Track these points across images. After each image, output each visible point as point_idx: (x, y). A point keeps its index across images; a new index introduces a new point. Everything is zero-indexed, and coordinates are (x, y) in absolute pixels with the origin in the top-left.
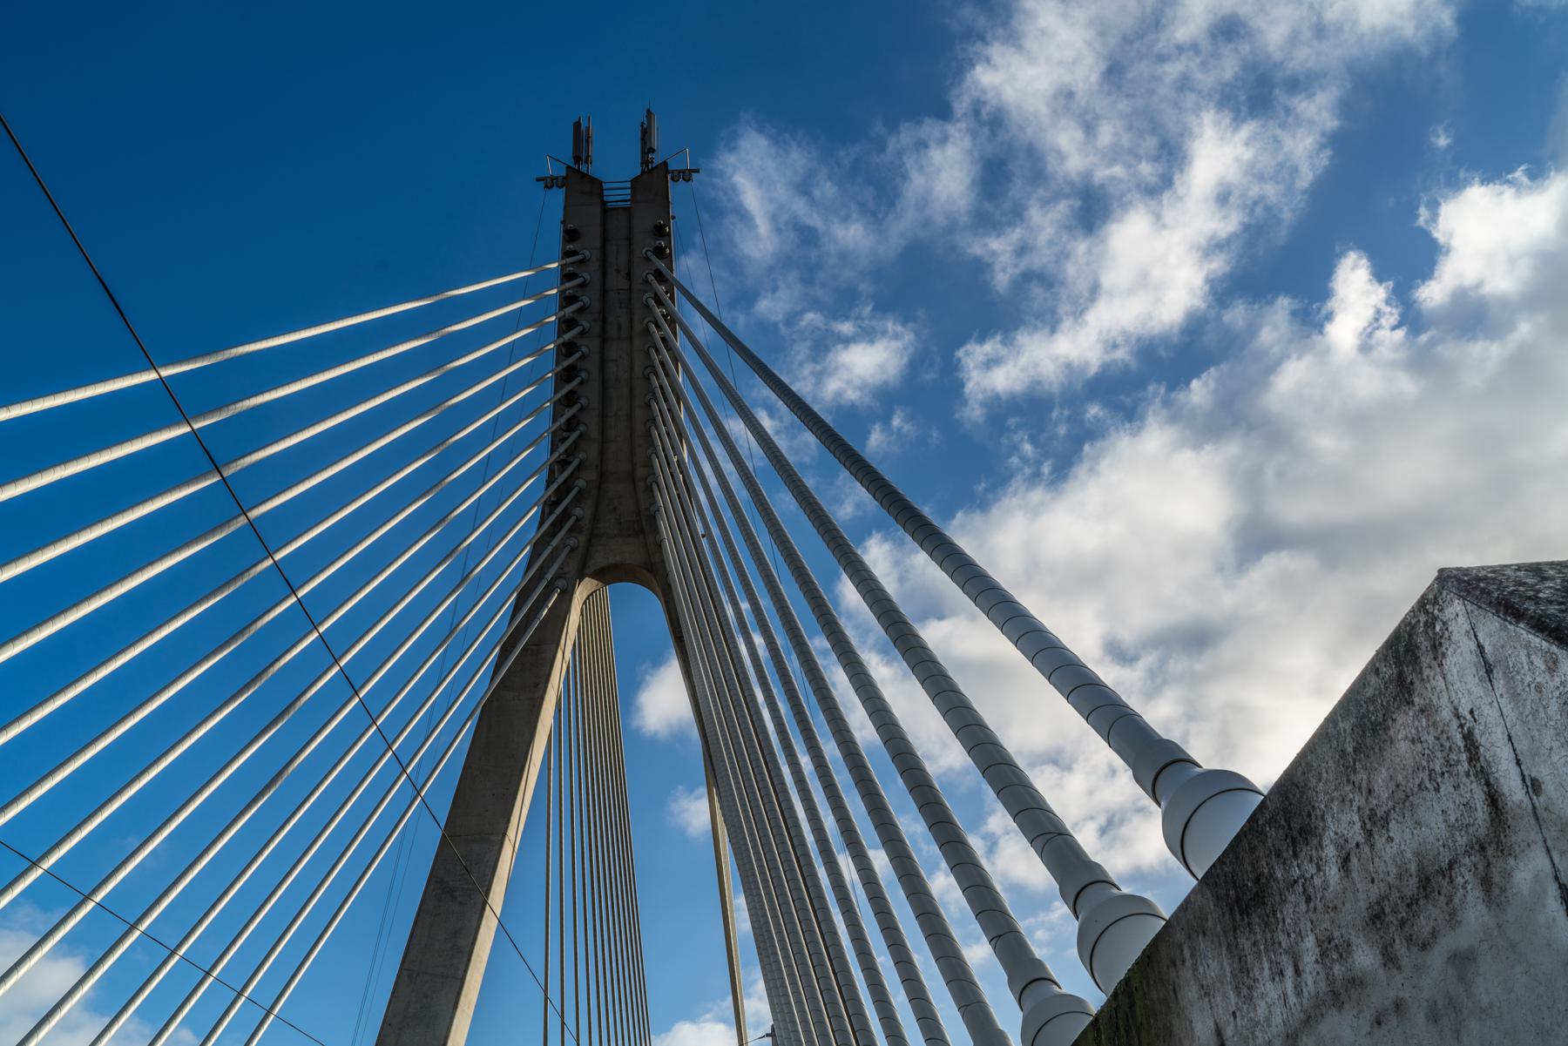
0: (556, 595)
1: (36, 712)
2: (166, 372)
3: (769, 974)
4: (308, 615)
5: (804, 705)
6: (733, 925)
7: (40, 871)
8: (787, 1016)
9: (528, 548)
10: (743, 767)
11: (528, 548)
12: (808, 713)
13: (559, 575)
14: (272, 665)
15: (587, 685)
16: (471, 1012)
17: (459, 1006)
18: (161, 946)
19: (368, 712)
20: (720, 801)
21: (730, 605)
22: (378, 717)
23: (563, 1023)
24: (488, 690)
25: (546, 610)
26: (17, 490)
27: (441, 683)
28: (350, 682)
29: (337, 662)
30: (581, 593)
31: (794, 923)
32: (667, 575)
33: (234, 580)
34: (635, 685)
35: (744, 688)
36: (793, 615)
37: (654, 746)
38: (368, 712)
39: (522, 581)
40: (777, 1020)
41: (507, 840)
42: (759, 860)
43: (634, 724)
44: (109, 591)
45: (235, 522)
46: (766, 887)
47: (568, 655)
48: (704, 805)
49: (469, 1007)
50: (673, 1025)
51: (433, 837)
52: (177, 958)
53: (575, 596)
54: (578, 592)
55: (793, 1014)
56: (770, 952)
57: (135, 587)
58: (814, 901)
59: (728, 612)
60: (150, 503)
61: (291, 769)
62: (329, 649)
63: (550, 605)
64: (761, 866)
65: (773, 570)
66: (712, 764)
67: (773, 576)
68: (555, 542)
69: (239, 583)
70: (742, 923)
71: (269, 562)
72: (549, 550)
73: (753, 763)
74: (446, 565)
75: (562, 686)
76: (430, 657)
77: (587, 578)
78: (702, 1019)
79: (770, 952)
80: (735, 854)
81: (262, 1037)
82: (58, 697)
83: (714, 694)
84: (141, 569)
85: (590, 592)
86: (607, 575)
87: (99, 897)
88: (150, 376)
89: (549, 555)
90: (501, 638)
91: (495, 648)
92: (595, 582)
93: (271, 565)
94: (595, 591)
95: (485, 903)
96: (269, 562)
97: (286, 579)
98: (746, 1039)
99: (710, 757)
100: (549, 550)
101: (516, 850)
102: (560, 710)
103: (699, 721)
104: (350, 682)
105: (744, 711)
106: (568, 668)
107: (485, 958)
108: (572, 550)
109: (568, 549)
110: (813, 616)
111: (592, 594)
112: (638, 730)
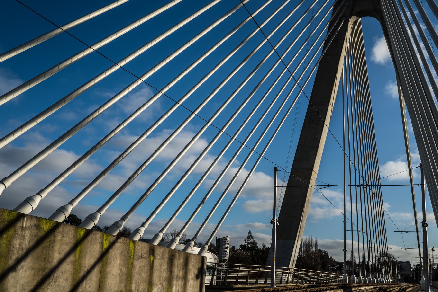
0: (343, 23)
1: (182, 74)
2: (59, 31)
3: (419, 144)
4: (264, 34)
5: (426, 37)
6: (412, 175)
7: (194, 115)
8: (428, 166)
9: (332, 7)
10: (413, 84)
11: (332, 7)
12: (428, 42)
13: (343, 16)
14: (253, 51)
15: (354, 53)
16: (321, 158)
17: (317, 156)
18: (229, 136)
19: (284, 64)
20: (402, 90)
21: (402, 12)
22: (288, 65)
23: (350, 160)
24: (326, 37)
25: (340, 28)
26: (144, 20)
27: (308, 52)
28: (278, 55)
29: (273, 48)
30: (351, 21)
31: (429, 130)
32: (382, 12)
33: (239, 25)
34: (370, 52)
35: (413, 54)
36: (430, 22)
37: (379, 66)
38: (284, 64)
39: (331, 19)
40: (423, 162)
41: (330, 105)
42: (416, 107)
43: (372, 59)
44: (209, 27)
45: (238, 6)
46: (418, 114)
47: (348, 43)
48: (396, 87)
49: (320, 156)
50: (387, 162)
51: (306, 103)
52: (234, 140)
53: (349, 22)
54: (350, 21)
55: (428, 159)
56: (422, 145)
57: (211, 30)
58: (432, 108)
59: (403, 14)
60: (202, 10)
61: (261, 83)
62: (271, 44)
63: (341, 26)
64: (417, 111)
65: (420, 2)
66: (400, 80)
67: (420, 4)
68: (341, 4)
69: (241, 26)
70: (410, 129)
71: (250, 18)
72: (340, 7)
73: (416, 81)
74: (305, 15)
75: (346, 53)
76: (302, 46)
77: (353, 16)
78: (397, 160)
79: (422, 145)
80: (408, 110)
81: (258, 165)
82: (176, 79)
83: (400, 53)
84: (189, 41)
85: (356, 20)
86: (360, 15)
87: (211, 122)
88: (65, 28)
89: (340, 9)
90: (325, 39)
91: (323, 42)
92: (356, 17)
93: (251, 19)
94: (356, 20)
95: (324, 123)
96: (250, 18)
97: (256, 22)
98: (411, 167)
99: (399, 75)
100: (340, 7)
101: (333, 108)
102: (346, 62)
103: (393, 60)
104: (278, 55)
105: (408, 49)
106: (348, 47)
107: (324, 141)
108: (347, 7)
109: (346, 6)
110: (431, 10)
111: (355, 21)
112: (373, 61)
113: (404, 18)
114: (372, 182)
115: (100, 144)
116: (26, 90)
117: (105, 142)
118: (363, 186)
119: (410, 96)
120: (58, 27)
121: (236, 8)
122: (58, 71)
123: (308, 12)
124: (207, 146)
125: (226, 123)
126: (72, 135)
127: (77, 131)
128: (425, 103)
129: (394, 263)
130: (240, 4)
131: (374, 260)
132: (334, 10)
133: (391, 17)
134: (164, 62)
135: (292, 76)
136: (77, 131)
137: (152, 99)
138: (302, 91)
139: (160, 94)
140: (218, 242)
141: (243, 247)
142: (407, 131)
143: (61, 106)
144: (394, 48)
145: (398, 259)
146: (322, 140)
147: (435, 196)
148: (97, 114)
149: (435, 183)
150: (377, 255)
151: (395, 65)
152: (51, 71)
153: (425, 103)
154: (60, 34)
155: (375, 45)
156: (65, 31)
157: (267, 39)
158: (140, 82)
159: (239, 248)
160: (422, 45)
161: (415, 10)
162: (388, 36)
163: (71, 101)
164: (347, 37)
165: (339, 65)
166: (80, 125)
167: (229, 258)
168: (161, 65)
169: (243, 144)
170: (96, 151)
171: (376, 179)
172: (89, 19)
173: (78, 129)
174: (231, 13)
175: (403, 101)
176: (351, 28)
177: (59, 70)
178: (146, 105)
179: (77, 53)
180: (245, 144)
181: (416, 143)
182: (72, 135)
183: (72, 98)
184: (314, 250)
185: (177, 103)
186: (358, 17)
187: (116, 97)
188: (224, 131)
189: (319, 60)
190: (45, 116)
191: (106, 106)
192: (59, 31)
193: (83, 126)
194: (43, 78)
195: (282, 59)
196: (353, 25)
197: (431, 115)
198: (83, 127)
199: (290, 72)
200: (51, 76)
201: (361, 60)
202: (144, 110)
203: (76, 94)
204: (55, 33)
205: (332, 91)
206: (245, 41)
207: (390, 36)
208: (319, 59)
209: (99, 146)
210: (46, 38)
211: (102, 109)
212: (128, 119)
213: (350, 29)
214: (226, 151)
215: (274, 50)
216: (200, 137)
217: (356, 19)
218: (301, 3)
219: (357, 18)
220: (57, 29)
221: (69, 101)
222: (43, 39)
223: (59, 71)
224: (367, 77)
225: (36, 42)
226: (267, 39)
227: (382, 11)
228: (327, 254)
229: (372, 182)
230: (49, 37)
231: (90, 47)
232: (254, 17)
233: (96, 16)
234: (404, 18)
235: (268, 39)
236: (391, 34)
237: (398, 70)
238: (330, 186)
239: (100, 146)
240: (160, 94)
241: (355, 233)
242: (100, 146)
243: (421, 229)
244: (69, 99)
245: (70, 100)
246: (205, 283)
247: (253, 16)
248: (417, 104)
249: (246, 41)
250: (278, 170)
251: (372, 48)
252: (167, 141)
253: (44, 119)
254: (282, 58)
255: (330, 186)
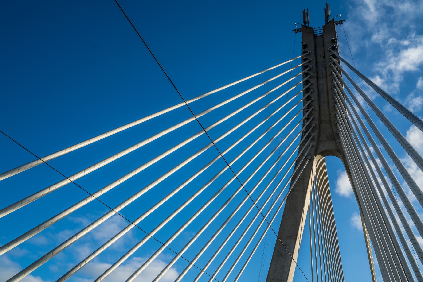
0: (308, 161)
2: (40, 162)
9: (298, 147)
11: (298, 147)
13: (308, 155)
18: (199, 269)
19: (252, 200)
24: (289, 192)
25: (305, 166)
28: (246, 191)
31: (381, 232)
34: (334, 185)
37: (343, 198)
41: (297, 239)
42: (379, 242)
43: (337, 191)
47: (313, 180)
51: (274, 238)
53: (314, 161)
54: (315, 160)
60: (168, 151)
63: (306, 164)
64: (372, 221)
66: (363, 213)
68: (307, 144)
71: (220, 156)
72: (305, 147)
75: (312, 189)
77: (318, 155)
83: (365, 198)
86: (324, 154)
91: (290, 178)
92: (320, 156)
94: (321, 159)
96: (220, 156)
100: (305, 147)
101: (301, 241)
102: (312, 197)
104: (246, 191)
106: (313, 184)
108: (312, 146)
111: (320, 160)
112: (338, 194)
113: (361, 154)
115: (69, 274)
116: (1, 217)
117: (74, 272)
119: (374, 232)
120: (38, 159)
121: (209, 146)
122: (35, 199)
123: (275, 151)
124: (178, 276)
125: (199, 253)
126: (43, 263)
127: (47, 260)
128: (380, 218)
130: (211, 143)
132: (299, 149)
133: (352, 159)
134: (110, 214)
135: (260, 212)
136: (48, 259)
137: (125, 230)
138: (270, 226)
139: (133, 226)
142: (373, 269)
143: (35, 234)
144: (356, 186)
146: (291, 273)
147: (386, 277)
148: (63, 247)
149: (387, 270)
151: (358, 201)
152: (28, 199)
153: (373, 202)
154: (41, 165)
155: (339, 178)
156: (45, 163)
157: (236, 176)
158: (113, 213)
160: (380, 180)
161: (370, 147)
162: (351, 174)
163: (45, 229)
164: (313, 174)
165: (306, 201)
166: (51, 254)
168: (139, 194)
169: (212, 277)
170: (65, 281)
172: (70, 151)
173: (49, 258)
174: (204, 150)
175: (368, 236)
176: (316, 166)
177: (36, 199)
178: (118, 235)
179: (61, 180)
180: (214, 277)
181: (381, 276)
182: (43, 263)
183: (46, 226)
185: (149, 235)
186: (322, 156)
187: (109, 214)
188: (194, 264)
189: (286, 196)
190: (24, 239)
191: (79, 236)
192: (40, 162)
193: (54, 255)
194: (20, 206)
195: (251, 196)
196: (317, 163)
197: (383, 223)
198: (54, 255)
199: (258, 208)
200: (28, 204)
201: (326, 196)
202: (112, 243)
203: (50, 223)
204: (36, 163)
205: (299, 225)
206: (216, 176)
207: (352, 174)
208: (287, 194)
209: (68, 276)
210: (26, 168)
211: (75, 239)
212: (104, 245)
213: (315, 167)
214: (201, 276)
215: (242, 187)
216: (172, 267)
217: (321, 158)
218: (269, 143)
219: (321, 157)
220: (38, 159)
221: (42, 229)
222: (24, 169)
223: (31, 202)
224: (335, 225)
225: (17, 171)
226: (236, 176)
227: (344, 151)
230: (30, 166)
231: (67, 178)
232: (223, 155)
233: (72, 151)
234: (361, 154)
235: (237, 176)
236: (351, 167)
237: (361, 206)
239: (70, 276)
240: (133, 226)
242: (70, 276)
244: (44, 227)
245: (44, 228)
247: (223, 154)
248: (380, 239)
249: (217, 177)
251: (337, 181)
252: (153, 256)
253: (15, 246)
254: (250, 195)
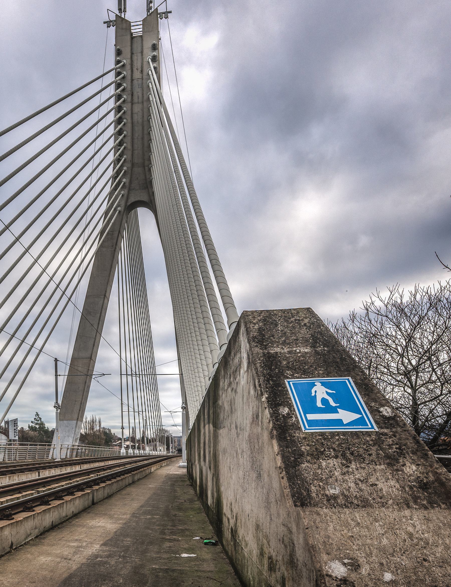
108: (123, 195)
114: (143, 371)
118: (135, 376)
129: (168, 438)
131: (152, 435)
140: (7, 425)
141: (31, 428)
145: (172, 434)
150: (154, 431)
159: (28, 429)
167: (19, 438)
171: (149, 368)
184: (98, 428)
228: (111, 431)
229: (143, 371)
238: (104, 375)
241: (131, 413)
243: (81, 410)
246: (142, 32)
250: (58, 361)
255: (104, 375)
